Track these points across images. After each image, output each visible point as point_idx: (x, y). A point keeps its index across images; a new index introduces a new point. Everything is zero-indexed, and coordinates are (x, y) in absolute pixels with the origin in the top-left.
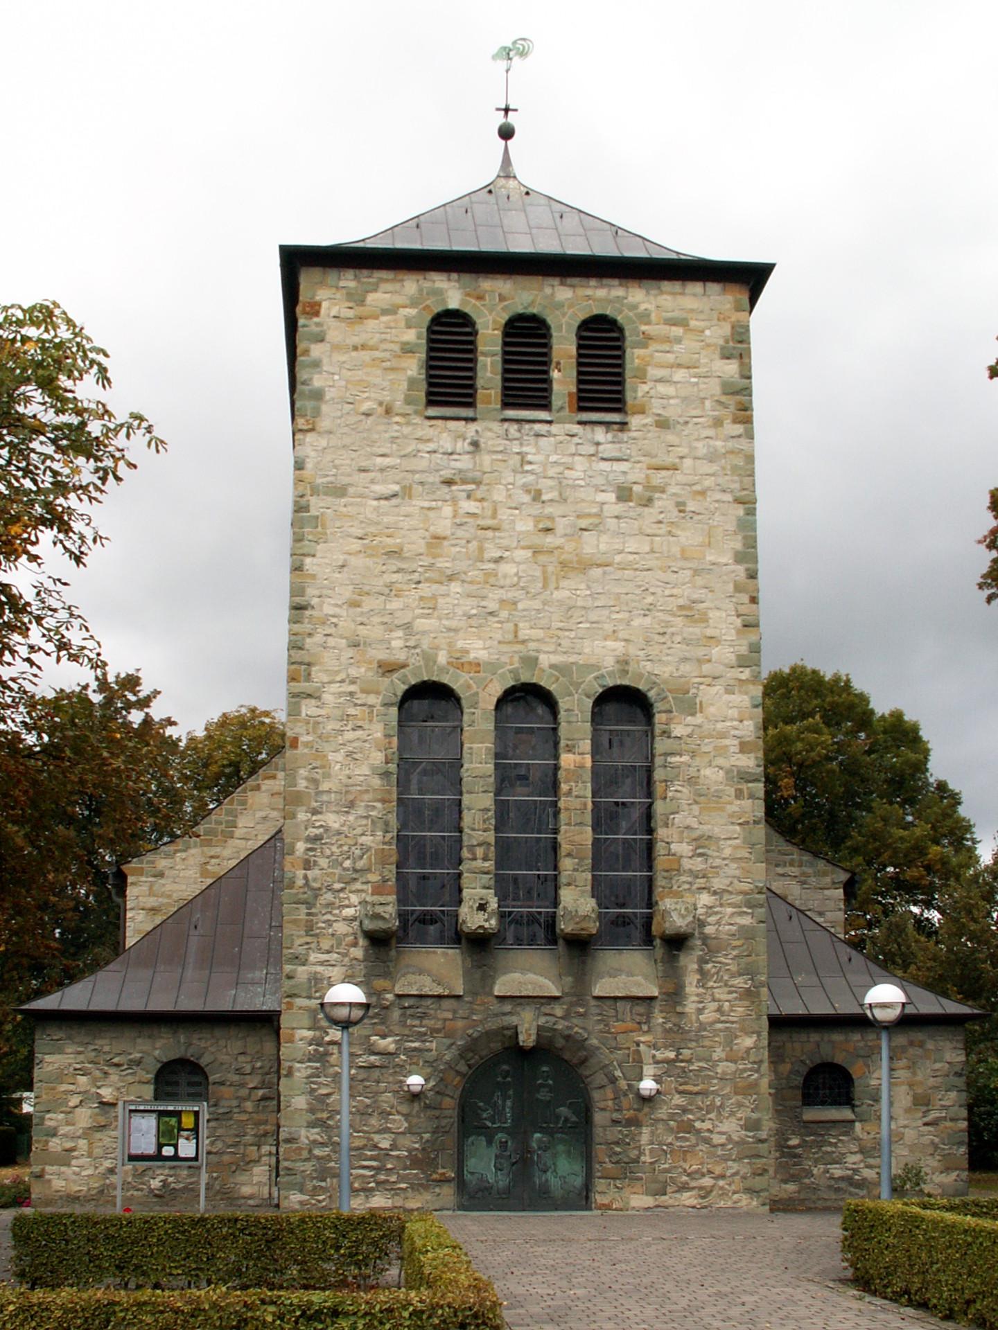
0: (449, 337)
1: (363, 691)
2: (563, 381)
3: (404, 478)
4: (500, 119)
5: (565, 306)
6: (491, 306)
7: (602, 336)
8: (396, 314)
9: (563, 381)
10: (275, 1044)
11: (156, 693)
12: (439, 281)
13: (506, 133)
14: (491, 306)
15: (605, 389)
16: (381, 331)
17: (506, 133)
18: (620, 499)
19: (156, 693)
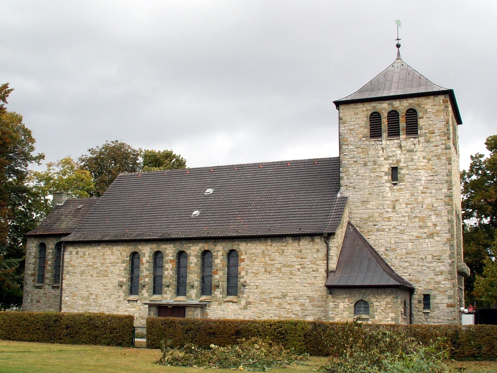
0: (375, 118)
1: (311, 264)
2: (403, 124)
3: (313, 260)
4: (397, 42)
5: (402, 106)
6: (384, 108)
7: (412, 114)
8: (361, 114)
9: (403, 124)
10: (340, 116)
11: (12, 90)
12: (374, 104)
13: (398, 46)
14: (384, 108)
15: (413, 129)
16: (359, 117)
17: (398, 46)
18: (423, 159)
19: (12, 90)
